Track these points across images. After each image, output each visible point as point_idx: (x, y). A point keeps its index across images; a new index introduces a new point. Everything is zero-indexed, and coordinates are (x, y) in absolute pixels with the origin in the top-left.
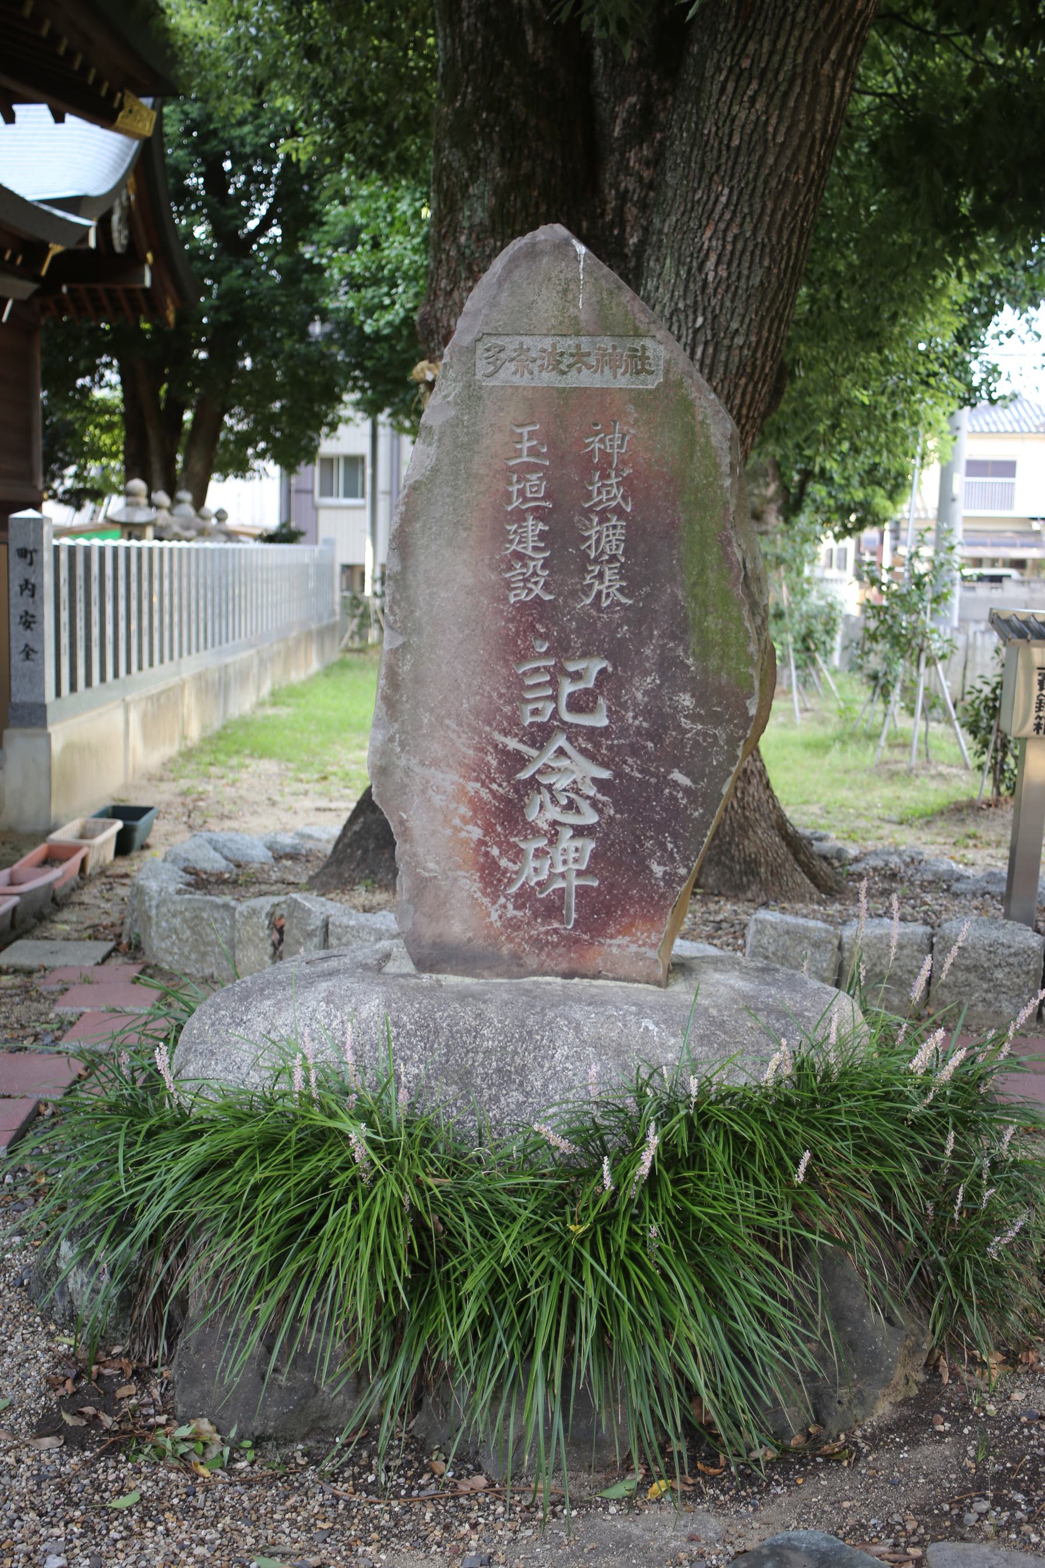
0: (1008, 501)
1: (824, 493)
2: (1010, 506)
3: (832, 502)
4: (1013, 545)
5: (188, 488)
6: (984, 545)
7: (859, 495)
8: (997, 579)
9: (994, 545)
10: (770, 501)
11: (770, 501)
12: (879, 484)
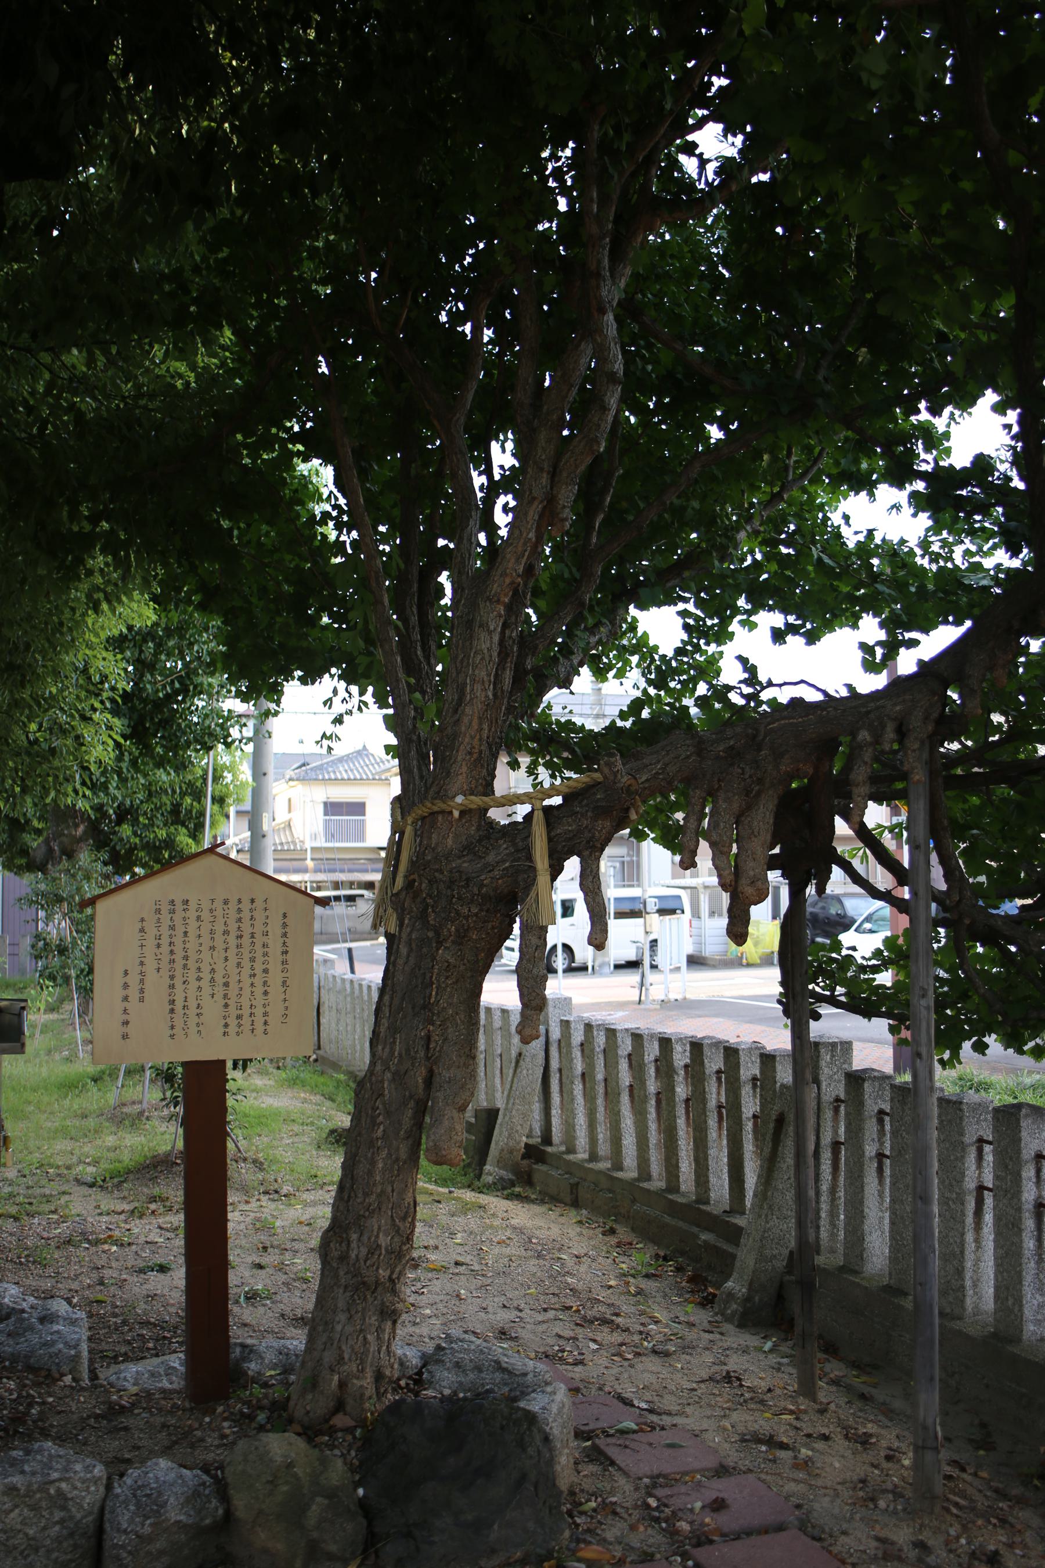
0: (361, 836)
1: (129, 833)
2: (363, 840)
3: (137, 840)
4: (366, 871)
5: (896, 984)
6: (342, 871)
7: (162, 834)
8: (351, 899)
9: (350, 871)
10: (80, 840)
11: (80, 840)
12: (183, 824)
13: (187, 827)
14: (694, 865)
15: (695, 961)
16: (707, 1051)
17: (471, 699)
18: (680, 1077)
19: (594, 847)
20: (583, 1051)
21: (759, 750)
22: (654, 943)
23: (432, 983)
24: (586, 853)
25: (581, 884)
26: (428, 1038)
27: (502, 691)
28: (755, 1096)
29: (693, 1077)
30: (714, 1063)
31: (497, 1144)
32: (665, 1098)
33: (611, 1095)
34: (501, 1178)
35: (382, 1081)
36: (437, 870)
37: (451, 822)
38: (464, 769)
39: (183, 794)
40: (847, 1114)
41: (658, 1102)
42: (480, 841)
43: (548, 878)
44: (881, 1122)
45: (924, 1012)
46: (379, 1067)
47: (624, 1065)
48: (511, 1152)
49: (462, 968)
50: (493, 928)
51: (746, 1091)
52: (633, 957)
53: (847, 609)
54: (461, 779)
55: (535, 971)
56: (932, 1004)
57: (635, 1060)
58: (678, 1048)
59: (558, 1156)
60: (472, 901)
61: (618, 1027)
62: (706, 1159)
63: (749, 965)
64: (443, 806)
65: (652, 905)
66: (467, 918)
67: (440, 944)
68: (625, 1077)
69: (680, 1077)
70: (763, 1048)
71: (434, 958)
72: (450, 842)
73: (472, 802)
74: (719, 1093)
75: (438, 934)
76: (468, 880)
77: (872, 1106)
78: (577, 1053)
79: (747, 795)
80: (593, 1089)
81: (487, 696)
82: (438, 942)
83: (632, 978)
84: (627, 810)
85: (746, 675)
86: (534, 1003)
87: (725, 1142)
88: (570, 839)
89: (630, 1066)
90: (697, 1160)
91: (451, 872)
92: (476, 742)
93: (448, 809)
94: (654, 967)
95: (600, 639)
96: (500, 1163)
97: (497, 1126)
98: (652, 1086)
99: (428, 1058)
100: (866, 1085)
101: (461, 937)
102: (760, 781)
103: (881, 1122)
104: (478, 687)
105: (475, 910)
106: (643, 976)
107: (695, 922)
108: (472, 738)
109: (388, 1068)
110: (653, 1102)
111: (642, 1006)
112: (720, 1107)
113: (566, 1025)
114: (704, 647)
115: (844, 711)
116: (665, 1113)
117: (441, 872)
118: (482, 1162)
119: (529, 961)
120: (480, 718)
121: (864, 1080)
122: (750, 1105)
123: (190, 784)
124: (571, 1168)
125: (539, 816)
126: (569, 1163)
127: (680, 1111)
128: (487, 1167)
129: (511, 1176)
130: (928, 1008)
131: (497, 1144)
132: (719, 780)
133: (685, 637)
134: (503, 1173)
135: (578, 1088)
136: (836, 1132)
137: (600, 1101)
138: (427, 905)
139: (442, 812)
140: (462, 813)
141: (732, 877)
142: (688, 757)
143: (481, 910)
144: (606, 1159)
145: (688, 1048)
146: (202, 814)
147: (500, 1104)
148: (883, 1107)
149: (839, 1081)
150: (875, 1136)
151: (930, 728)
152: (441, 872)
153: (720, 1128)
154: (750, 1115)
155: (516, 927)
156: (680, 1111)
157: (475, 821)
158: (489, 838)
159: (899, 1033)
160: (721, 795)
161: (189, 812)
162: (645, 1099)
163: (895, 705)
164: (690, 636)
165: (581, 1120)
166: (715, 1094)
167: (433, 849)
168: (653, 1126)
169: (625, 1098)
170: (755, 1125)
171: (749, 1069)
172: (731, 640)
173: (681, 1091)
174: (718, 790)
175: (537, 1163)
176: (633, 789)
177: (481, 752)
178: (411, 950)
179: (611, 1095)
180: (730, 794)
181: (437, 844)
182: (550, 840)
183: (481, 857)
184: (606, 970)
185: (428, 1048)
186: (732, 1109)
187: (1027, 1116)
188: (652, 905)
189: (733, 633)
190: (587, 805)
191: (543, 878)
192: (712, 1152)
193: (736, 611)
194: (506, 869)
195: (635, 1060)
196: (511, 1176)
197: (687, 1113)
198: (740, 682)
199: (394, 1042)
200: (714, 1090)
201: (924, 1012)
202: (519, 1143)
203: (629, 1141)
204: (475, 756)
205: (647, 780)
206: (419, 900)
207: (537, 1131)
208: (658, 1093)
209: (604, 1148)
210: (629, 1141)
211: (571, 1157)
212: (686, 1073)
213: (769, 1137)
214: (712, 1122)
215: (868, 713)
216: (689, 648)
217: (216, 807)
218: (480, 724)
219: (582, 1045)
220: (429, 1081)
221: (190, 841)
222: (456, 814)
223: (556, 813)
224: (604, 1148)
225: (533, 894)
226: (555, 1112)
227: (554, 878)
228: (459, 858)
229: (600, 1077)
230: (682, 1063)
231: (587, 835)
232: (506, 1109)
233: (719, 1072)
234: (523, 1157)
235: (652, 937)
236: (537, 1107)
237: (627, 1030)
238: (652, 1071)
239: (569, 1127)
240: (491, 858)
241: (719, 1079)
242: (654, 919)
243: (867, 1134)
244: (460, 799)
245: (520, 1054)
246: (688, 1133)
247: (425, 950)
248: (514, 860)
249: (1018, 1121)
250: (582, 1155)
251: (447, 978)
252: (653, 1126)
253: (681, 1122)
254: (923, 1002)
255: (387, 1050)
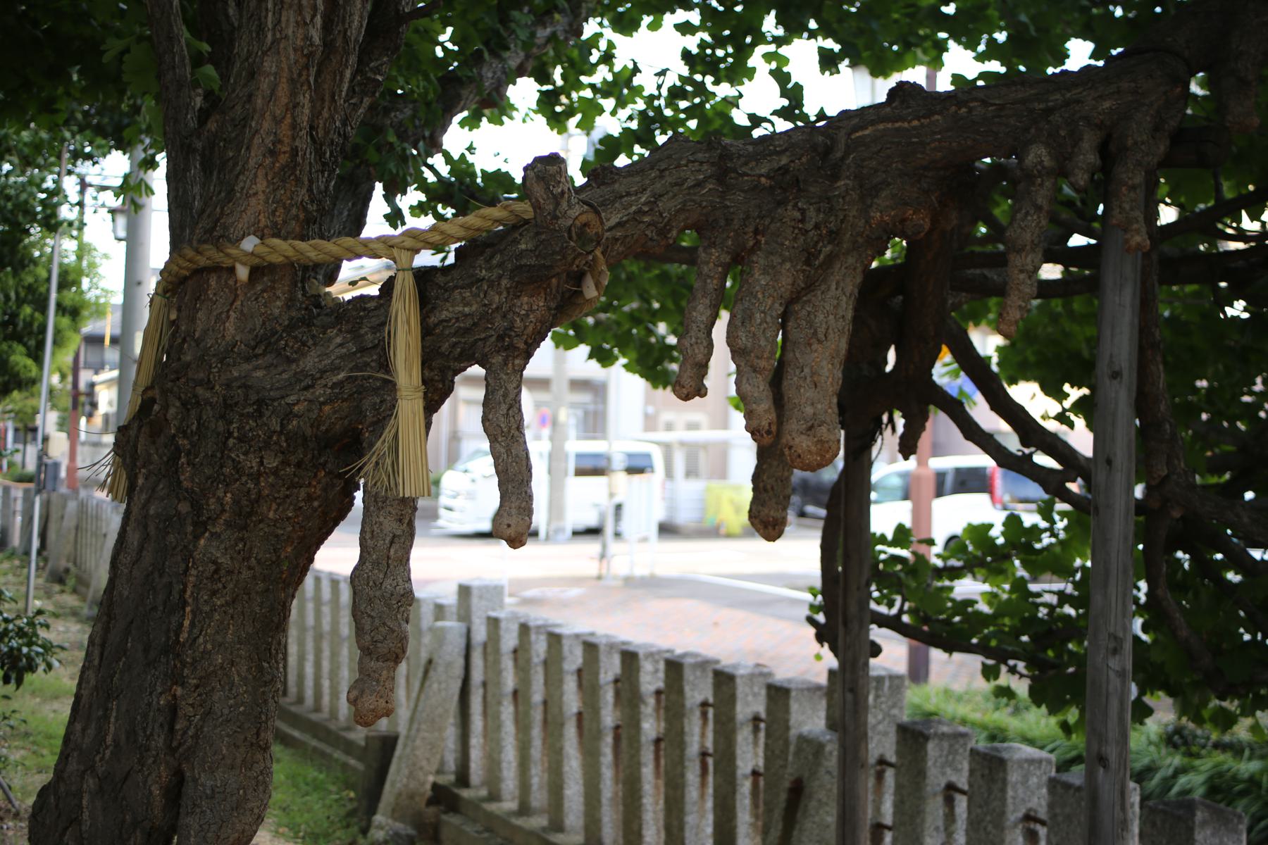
12: (20, 341)
13: (25, 345)
14: (701, 391)
15: (667, 530)
16: (688, 675)
17: (275, 41)
18: (648, 708)
19: (512, 347)
20: (516, 660)
21: (835, 177)
22: (619, 508)
23: (185, 603)
24: (497, 360)
25: (485, 420)
26: (173, 710)
27: (346, 40)
28: (756, 743)
29: (667, 709)
30: (698, 691)
31: (393, 785)
32: (626, 734)
33: (552, 725)
34: (397, 834)
35: (79, 794)
36: (200, 383)
37: (234, 291)
38: (261, 185)
39: (20, 302)
40: (899, 787)
41: (617, 739)
42: (291, 328)
43: (419, 405)
44: (949, 802)
45: (1115, 681)
46: (73, 766)
47: (570, 685)
48: (412, 796)
49: (246, 574)
50: (310, 498)
51: (743, 736)
52: (592, 521)
53: (926, 37)
54: (256, 204)
55: (388, 584)
56: (1129, 666)
57: (587, 677)
58: (647, 666)
59: (475, 805)
60: (267, 445)
61: (565, 631)
62: (681, 828)
63: (729, 536)
64: (218, 257)
65: (619, 462)
66: (255, 478)
67: (201, 526)
68: (572, 701)
69: (648, 708)
70: (770, 674)
71: (188, 555)
72: (230, 327)
73: (274, 249)
74: (703, 735)
75: (197, 507)
76: (260, 403)
77: (936, 778)
78: (508, 664)
79: (808, 262)
80: (527, 714)
81: (307, 38)
82: (195, 524)
83: (591, 547)
84: (579, 278)
85: (786, 102)
86: (382, 649)
87: (709, 804)
88: (467, 331)
89: (580, 685)
90: (668, 828)
91: (228, 386)
92: (284, 130)
93: (227, 262)
94: (617, 535)
95: (554, 35)
96: (396, 813)
97: (395, 761)
98: (609, 717)
99: (172, 750)
100: (931, 746)
101: (245, 516)
102: (834, 236)
103: (949, 802)
104: (289, 16)
105: (272, 462)
106: (604, 547)
107: (668, 485)
108: (278, 121)
109: (92, 768)
110: (609, 739)
111: (602, 582)
112: (704, 754)
113: (494, 623)
114: (710, 87)
115: (1002, 107)
116: (625, 757)
117: (209, 385)
118: (372, 810)
119: (376, 564)
120: (292, 81)
121: (927, 738)
122: (749, 755)
123: (30, 289)
124: (493, 824)
125: (406, 285)
126: (490, 816)
127: (647, 755)
128: (379, 818)
129: (411, 831)
130: (1122, 674)
131: (393, 785)
132: (756, 232)
133: (685, 71)
134: (399, 826)
135: (507, 711)
136: (877, 809)
137: (536, 732)
138: (178, 450)
139: (216, 269)
140: (256, 272)
141: (772, 416)
142: (699, 184)
143: (285, 463)
144: (541, 812)
145: (662, 666)
146: (43, 329)
147: (402, 729)
148: (954, 779)
149: (886, 734)
150: (940, 823)
151: (1162, 148)
152: (209, 385)
153: (703, 784)
154: (748, 770)
155: (359, 495)
156: (647, 755)
157: (282, 291)
158: (309, 324)
159: (996, 677)
160: (760, 259)
161: (28, 324)
162: (598, 735)
163: (1101, 97)
164: (692, 71)
165: (510, 755)
166: (698, 736)
167: (198, 342)
168: (607, 773)
169: (571, 731)
170: (755, 785)
171: (750, 704)
172: (750, 79)
173: (650, 727)
174: (752, 251)
175: (445, 812)
176: (591, 232)
177: (294, 152)
178: (146, 537)
179: (552, 725)
180: (776, 260)
181: (205, 332)
182: (426, 331)
183: (290, 361)
184: (561, 537)
185: (172, 729)
186: (722, 759)
187: (1204, 823)
188: (619, 462)
189: (754, 70)
190: (500, 265)
191: (409, 405)
192: (690, 819)
193: (760, 38)
194: (340, 384)
195: (587, 677)
196: (411, 831)
197: (657, 759)
198: (775, 113)
199: (106, 717)
200: (697, 730)
201: (1115, 681)
202: (423, 784)
203: (574, 792)
204: (283, 159)
205: (620, 224)
206: (162, 439)
207: (451, 765)
208: (617, 728)
209: (539, 798)
210: (574, 792)
211: (492, 807)
212: (658, 701)
213: (778, 814)
214: (692, 776)
215: (1048, 111)
216: (689, 88)
217: (65, 321)
218: (293, 94)
219: (515, 651)
220: (175, 792)
221: (29, 362)
222: (243, 273)
223: (440, 279)
224: (539, 798)
225: (388, 434)
226: (476, 741)
227: (432, 406)
228: (248, 359)
229: (537, 697)
230: (652, 688)
231: (500, 324)
232: (407, 737)
233: (704, 704)
234: (431, 802)
235: (617, 500)
236: (451, 733)
237: (577, 636)
238: (609, 696)
239: (493, 764)
240: (310, 362)
241: (704, 715)
242: (620, 479)
243: (929, 819)
244: (250, 243)
245: (430, 662)
246: (656, 787)
247: (171, 538)
248: (357, 368)
249: (1191, 830)
250: (509, 805)
251: (214, 593)
252: (607, 773)
253: (648, 772)
254: (1114, 663)
255: (91, 731)
